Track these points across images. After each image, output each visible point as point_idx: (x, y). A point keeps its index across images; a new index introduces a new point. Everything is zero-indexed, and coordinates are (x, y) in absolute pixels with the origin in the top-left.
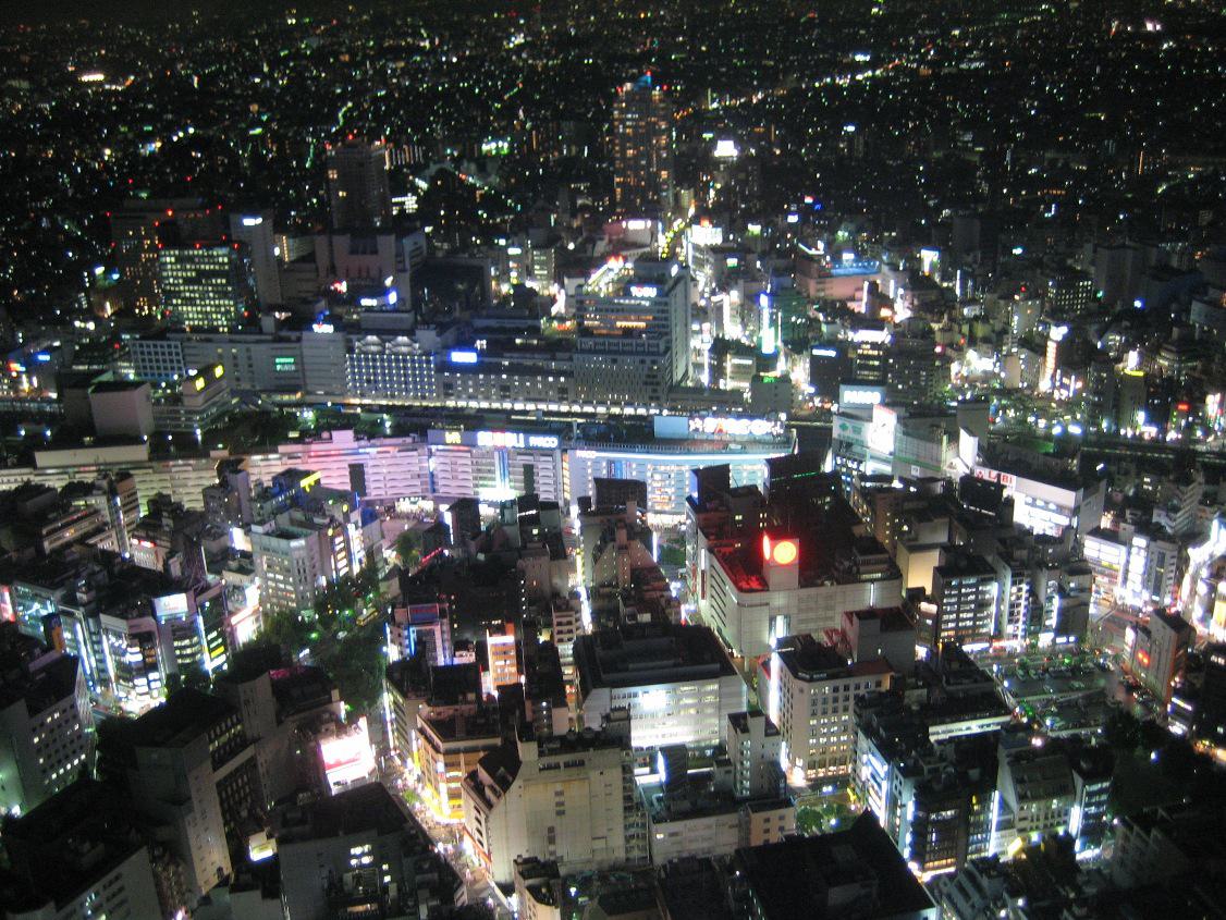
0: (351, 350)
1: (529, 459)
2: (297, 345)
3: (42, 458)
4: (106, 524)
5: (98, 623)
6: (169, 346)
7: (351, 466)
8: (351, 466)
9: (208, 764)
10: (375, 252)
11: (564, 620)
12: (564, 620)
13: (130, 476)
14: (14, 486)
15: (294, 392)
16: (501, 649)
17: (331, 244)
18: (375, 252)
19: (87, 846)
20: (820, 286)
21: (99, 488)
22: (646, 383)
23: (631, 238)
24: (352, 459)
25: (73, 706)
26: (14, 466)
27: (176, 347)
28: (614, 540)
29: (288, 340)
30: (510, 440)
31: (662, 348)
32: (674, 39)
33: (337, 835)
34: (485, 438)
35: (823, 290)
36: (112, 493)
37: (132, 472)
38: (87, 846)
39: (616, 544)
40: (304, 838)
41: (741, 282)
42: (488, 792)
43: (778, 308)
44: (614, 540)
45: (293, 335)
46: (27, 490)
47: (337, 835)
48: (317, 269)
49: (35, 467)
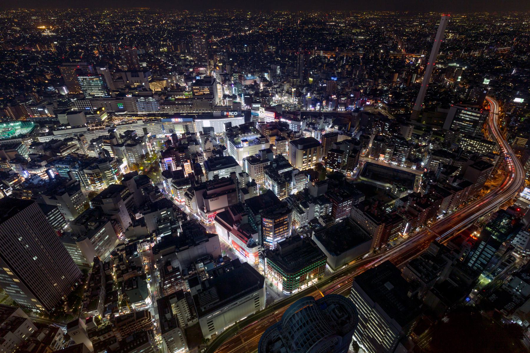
0: (137, 101)
5: (83, 172)
15: (124, 112)
23: (201, 72)
29: (120, 99)
30: (180, 120)
34: (173, 120)
36: (79, 140)
40: (149, 213)
45: (121, 98)
46: (53, 141)
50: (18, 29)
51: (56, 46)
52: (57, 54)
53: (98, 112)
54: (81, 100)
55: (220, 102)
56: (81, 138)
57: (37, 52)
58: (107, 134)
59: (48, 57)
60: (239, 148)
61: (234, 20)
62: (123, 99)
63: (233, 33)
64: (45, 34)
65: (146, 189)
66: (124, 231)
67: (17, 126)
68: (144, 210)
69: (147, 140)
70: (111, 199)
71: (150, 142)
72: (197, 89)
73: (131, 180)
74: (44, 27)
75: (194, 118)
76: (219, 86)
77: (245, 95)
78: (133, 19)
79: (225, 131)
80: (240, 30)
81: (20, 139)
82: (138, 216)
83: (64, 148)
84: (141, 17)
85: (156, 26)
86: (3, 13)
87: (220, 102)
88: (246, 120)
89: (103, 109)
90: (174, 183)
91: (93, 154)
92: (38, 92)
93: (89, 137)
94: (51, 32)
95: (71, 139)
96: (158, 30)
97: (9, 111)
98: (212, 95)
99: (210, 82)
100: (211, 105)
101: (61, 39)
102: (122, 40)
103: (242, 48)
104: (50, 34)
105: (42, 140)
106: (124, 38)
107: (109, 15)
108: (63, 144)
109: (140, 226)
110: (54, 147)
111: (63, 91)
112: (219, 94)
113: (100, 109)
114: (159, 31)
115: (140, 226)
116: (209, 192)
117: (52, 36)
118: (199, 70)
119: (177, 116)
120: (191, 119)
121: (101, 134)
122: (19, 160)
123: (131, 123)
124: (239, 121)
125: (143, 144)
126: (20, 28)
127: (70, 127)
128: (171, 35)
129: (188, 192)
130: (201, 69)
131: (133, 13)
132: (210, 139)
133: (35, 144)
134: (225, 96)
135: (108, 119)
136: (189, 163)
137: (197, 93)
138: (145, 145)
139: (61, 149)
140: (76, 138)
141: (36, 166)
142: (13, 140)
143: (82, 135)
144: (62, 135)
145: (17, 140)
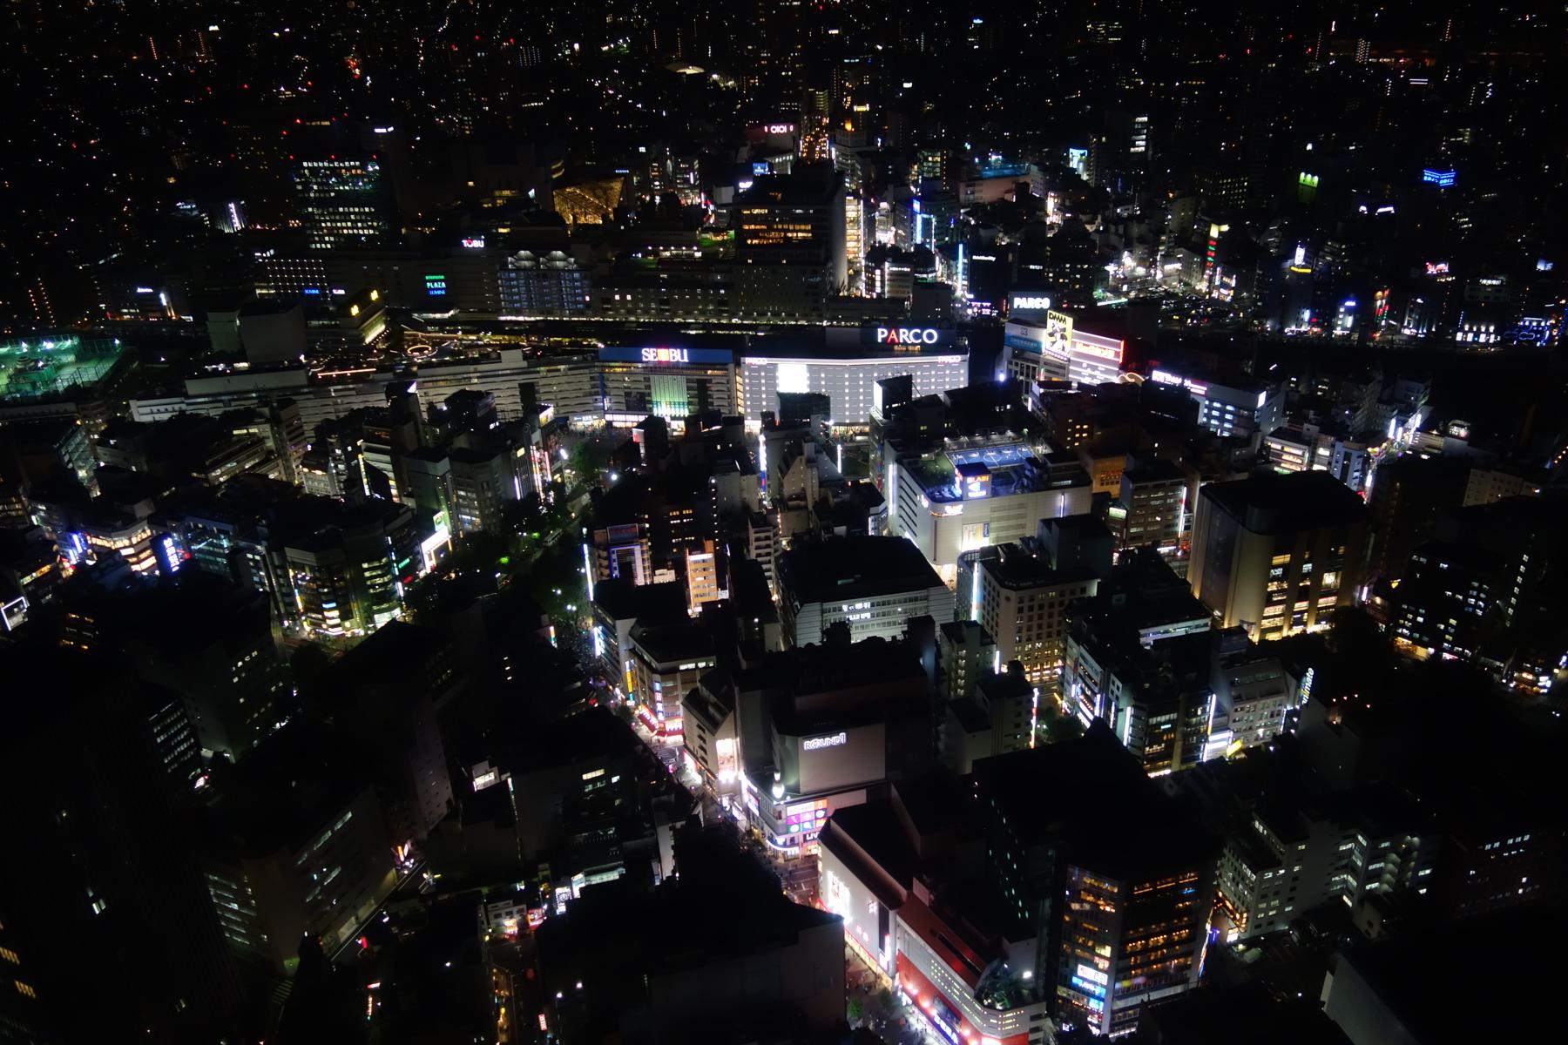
4: (271, 452)
5: (283, 556)
6: (310, 265)
7: (521, 385)
8: (521, 385)
11: (762, 535)
12: (762, 535)
13: (294, 402)
14: (166, 417)
21: (261, 415)
24: (522, 379)
27: (318, 265)
34: (650, 355)
36: (274, 421)
37: (525, 364)
39: (804, 458)
41: (890, 187)
42: (711, 710)
49: (187, 396)
53: (355, 310)
56: (284, 414)
60: (944, 500)
69: (537, 436)
75: (739, 348)
79: (878, 416)
81: (71, 407)
90: (640, 640)
95: (247, 418)
97: (37, 296)
105: (144, 412)
112: (854, 245)
116: (801, 702)
119: (666, 336)
123: (475, 361)
124: (944, 374)
129: (705, 692)
132: (808, 448)
133: (123, 428)
134: (877, 255)
136: (709, 556)
137: (754, 235)
138: (527, 461)
140: (266, 410)
144: (215, 397)
145: (61, 407)
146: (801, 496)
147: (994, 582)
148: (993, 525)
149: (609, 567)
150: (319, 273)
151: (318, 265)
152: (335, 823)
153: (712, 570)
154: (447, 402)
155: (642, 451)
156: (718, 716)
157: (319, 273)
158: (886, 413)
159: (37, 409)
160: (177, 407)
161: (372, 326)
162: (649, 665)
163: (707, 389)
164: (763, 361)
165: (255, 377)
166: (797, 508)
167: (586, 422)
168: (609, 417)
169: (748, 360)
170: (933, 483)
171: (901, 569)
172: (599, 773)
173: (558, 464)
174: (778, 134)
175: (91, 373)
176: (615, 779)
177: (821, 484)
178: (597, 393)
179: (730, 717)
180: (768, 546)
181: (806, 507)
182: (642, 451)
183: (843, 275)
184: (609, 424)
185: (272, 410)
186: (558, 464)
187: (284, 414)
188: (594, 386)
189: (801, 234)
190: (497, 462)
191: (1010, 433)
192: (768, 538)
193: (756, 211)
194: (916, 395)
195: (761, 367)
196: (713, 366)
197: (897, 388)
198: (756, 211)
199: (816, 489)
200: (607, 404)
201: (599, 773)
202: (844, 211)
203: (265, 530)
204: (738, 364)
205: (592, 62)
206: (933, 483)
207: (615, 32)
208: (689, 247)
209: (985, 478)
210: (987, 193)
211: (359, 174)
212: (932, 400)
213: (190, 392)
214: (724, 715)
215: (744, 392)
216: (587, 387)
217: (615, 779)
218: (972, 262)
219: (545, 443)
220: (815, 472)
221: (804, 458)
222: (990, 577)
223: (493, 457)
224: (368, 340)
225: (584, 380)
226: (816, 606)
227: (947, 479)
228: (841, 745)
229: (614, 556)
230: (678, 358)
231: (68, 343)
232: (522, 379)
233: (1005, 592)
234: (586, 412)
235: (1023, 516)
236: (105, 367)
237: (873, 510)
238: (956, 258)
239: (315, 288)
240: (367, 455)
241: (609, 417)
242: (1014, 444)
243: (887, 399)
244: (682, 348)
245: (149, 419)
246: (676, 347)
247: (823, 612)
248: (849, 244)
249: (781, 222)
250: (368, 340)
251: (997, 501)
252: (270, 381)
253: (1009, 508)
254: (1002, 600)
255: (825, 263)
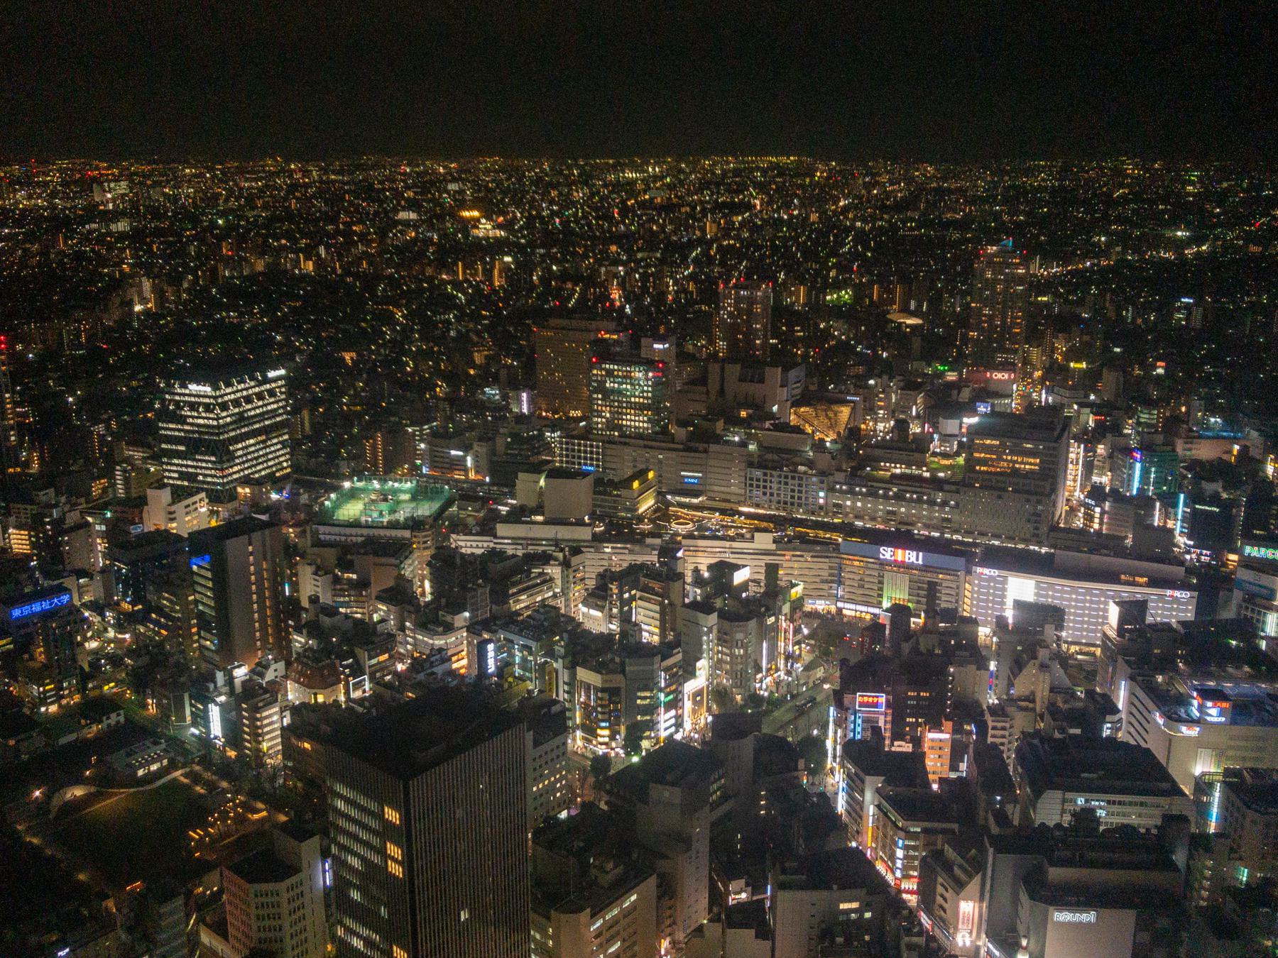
1: (929, 577)
2: (704, 455)
3: (502, 529)
6: (592, 446)
7: (767, 565)
8: (767, 565)
9: (707, 808)
10: (762, 381)
11: (999, 725)
12: (999, 725)
14: (479, 551)
15: (697, 496)
16: (938, 744)
17: (723, 369)
18: (762, 381)
19: (611, 865)
20: (1188, 446)
21: (556, 559)
22: (1029, 521)
23: (992, 387)
24: (768, 559)
25: (565, 744)
26: (478, 534)
27: (598, 447)
28: (1036, 658)
29: (696, 451)
30: (911, 557)
31: (1048, 489)
32: (552, 263)
33: (830, 888)
34: (887, 553)
35: (1190, 450)
36: (566, 564)
37: (773, 547)
38: (611, 865)
39: (1037, 662)
40: (801, 887)
41: (1109, 436)
42: (957, 871)
43: (1151, 462)
44: (1036, 658)
45: (701, 446)
46: (494, 555)
47: (830, 888)
48: (708, 393)
49: (495, 537)
50: (413, 216)
51: (506, 269)
52: (505, 291)
53: (636, 484)
54: (580, 438)
55: (1072, 511)
56: (575, 560)
57: (457, 285)
58: (652, 558)
59: (480, 298)
60: (1180, 720)
61: (1125, 200)
62: (706, 451)
63: (1124, 252)
64: (480, 233)
65: (777, 795)
66: (680, 936)
67: (405, 492)
68: (784, 871)
69: (786, 608)
70: (677, 791)
71: (792, 620)
72: (988, 449)
73: (744, 741)
74: (476, 214)
75: (967, 556)
76: (1076, 452)
77: (1194, 498)
78: (738, 192)
79: (1112, 634)
80: (1159, 242)
81: (407, 534)
82: (739, 895)
83: (520, 582)
84: (761, 187)
85: (814, 217)
86: (1132, 178)
87: (1072, 511)
88: (1199, 611)
89: (651, 475)
90: (888, 798)
91: (595, 620)
92: (451, 399)
93: (592, 565)
94: (494, 228)
95: (545, 559)
96: (818, 231)
98: (1050, 476)
99: (1050, 427)
100: (1036, 518)
101: (521, 249)
102: (697, 261)
103: (1165, 309)
104: (491, 234)
106: (706, 253)
107: (662, 178)
108: (520, 570)
109: (752, 932)
110: (502, 574)
111: (519, 402)
112: (1073, 486)
113: (641, 474)
114: (823, 234)
115: (752, 932)
116: (1055, 874)
117: (495, 238)
118: (987, 381)
119: (903, 539)
120: (961, 561)
121: (640, 559)
122: (399, 595)
123: (732, 539)
124: (1173, 607)
125: (773, 619)
126: (419, 214)
127: (540, 518)
128: (867, 247)
130: (999, 376)
131: (737, 173)
132: (1043, 654)
134: (1097, 493)
135: (655, 511)
137: (984, 462)
138: (775, 628)
139: (514, 584)
140: (560, 555)
141: (437, 622)
142: (389, 533)
143: (576, 551)
144: (516, 540)
146: (1031, 698)
147: (1238, 803)
148: (1230, 753)
149: (854, 730)
150: (598, 453)
151: (598, 447)
152: (624, 902)
153: (947, 750)
154: (710, 567)
155: (887, 632)
156: (963, 877)
157: (598, 453)
158: (1121, 631)
159: (382, 532)
160: (485, 545)
161: (645, 499)
162: (894, 823)
163: (936, 591)
164: (994, 572)
165: (547, 527)
166: (1026, 709)
167: (821, 606)
168: (840, 605)
169: (979, 570)
170: (1172, 705)
171: (1142, 772)
172: (855, 905)
173: (799, 637)
174: (999, 380)
175: (426, 509)
176: (868, 915)
177: (1052, 690)
178: (832, 582)
179: (977, 879)
180: (1003, 737)
181: (1034, 710)
182: (887, 632)
183: (1062, 508)
184: (840, 610)
185: (565, 556)
186: (799, 637)
187: (575, 560)
188: (831, 575)
189: (1030, 464)
190: (752, 624)
191: (1247, 669)
192: (1003, 729)
193: (988, 442)
194: (1149, 620)
195: (991, 578)
196: (946, 571)
197: (1133, 611)
198: (988, 442)
199: (1046, 693)
200: (840, 593)
201: (855, 905)
202: (1068, 452)
203: (562, 650)
204: (969, 572)
205: (818, 309)
206: (1172, 705)
207: (837, 286)
208: (919, 467)
209: (1225, 705)
210: (1205, 451)
211: (640, 382)
212: (1167, 627)
213: (499, 534)
214: (971, 877)
215: (972, 599)
216: (825, 574)
217: (868, 915)
218: (1194, 511)
219: (792, 616)
220: (1047, 676)
221: (1037, 662)
222: (1233, 797)
223: (748, 619)
224: (641, 511)
225: (823, 567)
226: (1058, 794)
227: (1183, 701)
228: (1089, 923)
229: (859, 721)
230: (913, 559)
231: (409, 485)
232: (768, 559)
233: (1250, 814)
234: (820, 597)
235: (1261, 749)
236: (436, 505)
237: (1109, 718)
238: (1175, 505)
239: (592, 465)
240: (640, 602)
241: (840, 605)
242: (1252, 678)
243: (1122, 620)
244: (918, 550)
245: (469, 551)
246: (912, 550)
247: (1064, 801)
248: (1068, 483)
249: (1012, 453)
250: (641, 511)
251: (1236, 730)
252: (564, 533)
253: (1246, 739)
254: (1247, 823)
255: (1049, 495)
